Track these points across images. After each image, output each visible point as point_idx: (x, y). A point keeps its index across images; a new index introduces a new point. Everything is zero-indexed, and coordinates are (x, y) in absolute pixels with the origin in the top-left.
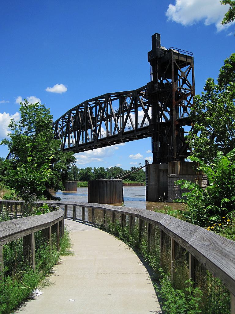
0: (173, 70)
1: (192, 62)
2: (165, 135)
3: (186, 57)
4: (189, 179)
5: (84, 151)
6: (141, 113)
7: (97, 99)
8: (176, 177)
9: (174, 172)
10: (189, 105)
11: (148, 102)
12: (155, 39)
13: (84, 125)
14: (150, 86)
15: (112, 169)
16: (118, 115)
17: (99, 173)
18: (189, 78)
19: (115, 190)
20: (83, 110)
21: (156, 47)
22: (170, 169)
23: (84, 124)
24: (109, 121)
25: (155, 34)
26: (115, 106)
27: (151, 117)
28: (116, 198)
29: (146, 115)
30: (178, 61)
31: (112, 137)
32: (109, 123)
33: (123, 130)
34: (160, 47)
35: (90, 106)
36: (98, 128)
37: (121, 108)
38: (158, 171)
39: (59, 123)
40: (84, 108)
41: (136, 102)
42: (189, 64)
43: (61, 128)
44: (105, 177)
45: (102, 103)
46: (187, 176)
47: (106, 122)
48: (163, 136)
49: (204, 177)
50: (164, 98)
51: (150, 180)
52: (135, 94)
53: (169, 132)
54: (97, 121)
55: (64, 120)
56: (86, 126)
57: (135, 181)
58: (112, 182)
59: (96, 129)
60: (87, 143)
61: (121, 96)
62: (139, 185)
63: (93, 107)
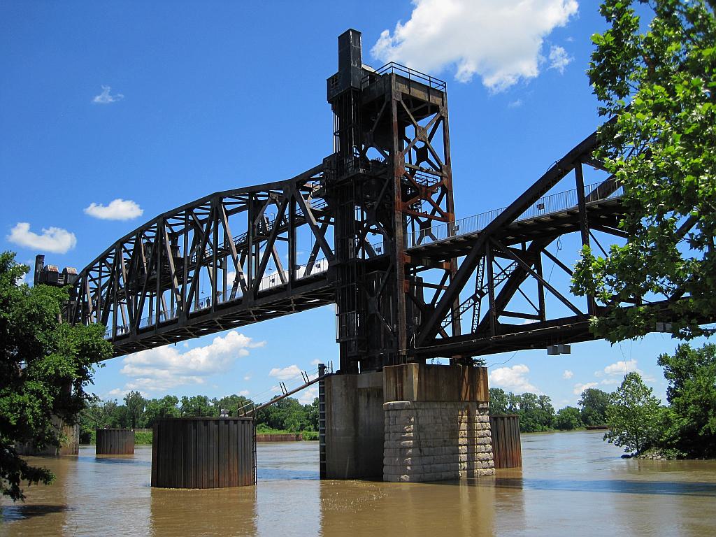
0: (395, 120)
1: (443, 105)
2: (372, 294)
3: (429, 90)
4: (443, 414)
5: (152, 347)
6: (305, 236)
7: (189, 209)
8: (408, 409)
9: (402, 396)
10: (437, 214)
11: (325, 212)
12: (348, 45)
13: (153, 277)
14: (333, 166)
15: (226, 401)
16: (244, 248)
18: (437, 144)
19: (232, 447)
20: (152, 240)
21: (350, 62)
22: (389, 387)
24: (220, 267)
25: (348, 32)
26: (237, 226)
27: (332, 247)
28: (236, 471)
29: (321, 243)
30: (409, 100)
31: (226, 306)
32: (220, 271)
33: (258, 287)
34: (359, 64)
35: (171, 230)
36: (189, 286)
37: (253, 229)
38: (354, 395)
39: (91, 276)
40: (154, 234)
41: (293, 209)
42: (435, 109)
43: (96, 290)
45: (202, 222)
46: (436, 406)
47: (211, 268)
48: (369, 297)
49: (483, 408)
50: (368, 196)
51: (333, 419)
52: (291, 191)
53: (385, 285)
54: (188, 265)
55: (105, 269)
56: (158, 279)
57: (280, 429)
58: (223, 423)
59: (184, 289)
60: (160, 325)
61: (252, 200)
62: (292, 440)
63: (180, 233)
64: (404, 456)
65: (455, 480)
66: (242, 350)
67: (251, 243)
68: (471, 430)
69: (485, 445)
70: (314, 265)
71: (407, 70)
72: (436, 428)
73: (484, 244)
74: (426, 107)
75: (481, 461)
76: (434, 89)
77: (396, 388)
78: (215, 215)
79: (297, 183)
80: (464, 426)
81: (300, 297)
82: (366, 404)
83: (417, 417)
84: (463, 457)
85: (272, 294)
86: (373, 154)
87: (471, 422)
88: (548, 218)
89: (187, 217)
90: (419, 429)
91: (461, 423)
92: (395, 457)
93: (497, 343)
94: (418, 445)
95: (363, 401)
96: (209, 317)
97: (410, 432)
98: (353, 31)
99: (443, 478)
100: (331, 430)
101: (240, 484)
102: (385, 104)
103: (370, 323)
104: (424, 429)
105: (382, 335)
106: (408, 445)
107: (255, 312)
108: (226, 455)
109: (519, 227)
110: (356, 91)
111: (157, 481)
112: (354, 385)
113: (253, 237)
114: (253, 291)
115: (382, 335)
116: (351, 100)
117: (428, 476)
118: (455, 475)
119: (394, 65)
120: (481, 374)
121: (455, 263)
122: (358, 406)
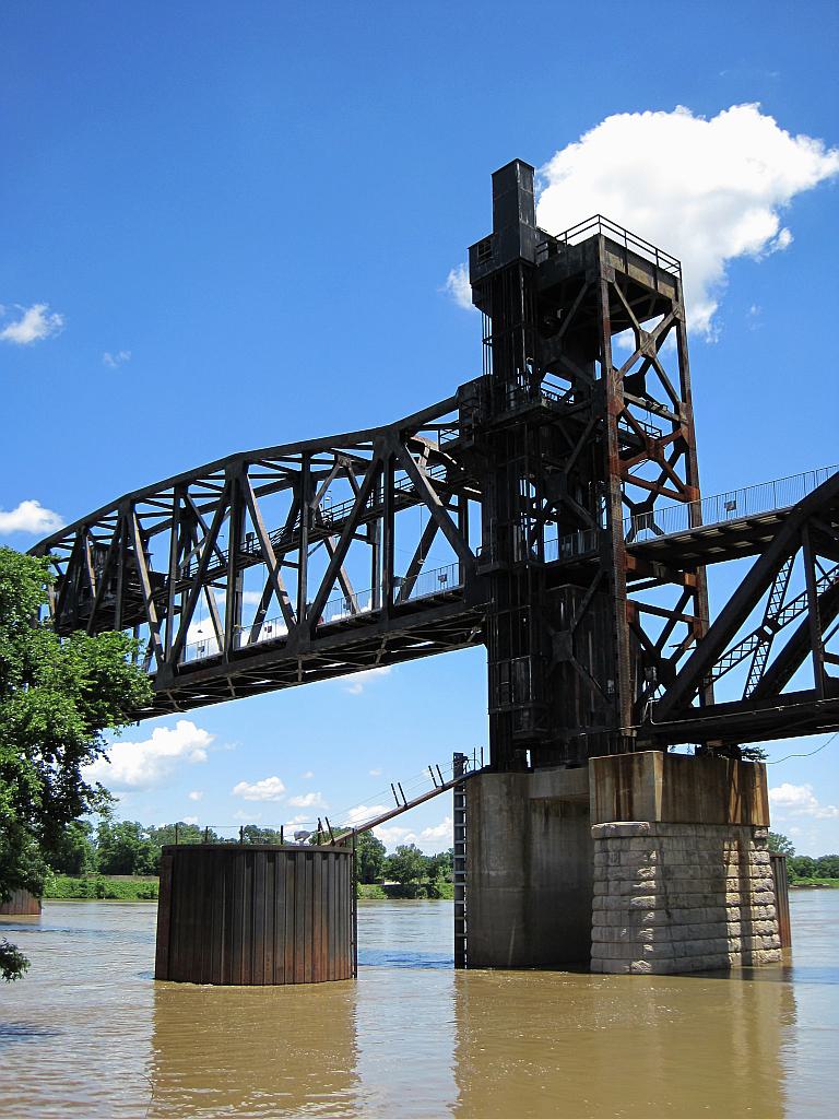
1: (677, 300)
3: (655, 270)
7: (181, 484)
8: (645, 836)
9: (631, 812)
10: (669, 484)
13: (107, 604)
14: (478, 399)
17: (120, 845)
22: (602, 795)
23: (108, 599)
25: (513, 163)
26: (272, 513)
28: (325, 951)
33: (317, 616)
38: (523, 809)
40: (112, 532)
42: (663, 305)
44: (141, 862)
48: (552, 632)
51: (483, 857)
52: (397, 441)
64: (637, 925)
65: (723, 970)
66: (197, 751)
67: (173, 588)
68: (744, 877)
69: (765, 905)
70: (263, 629)
71: (622, 233)
72: (691, 872)
73: (799, 531)
74: (649, 301)
75: (761, 935)
76: (663, 271)
77: (618, 796)
78: (233, 493)
79: (402, 433)
80: (733, 870)
81: (402, 635)
82: (543, 830)
83: (661, 853)
84: (735, 928)
85: (266, 651)
86: (555, 386)
87: (743, 862)
88: (716, 532)
89: (177, 503)
90: (666, 874)
91: (728, 864)
92: (621, 926)
93: (828, 711)
94: (665, 905)
95: (537, 822)
96: (218, 672)
97: (649, 879)
98: (522, 164)
99: (704, 967)
100: (480, 874)
101: (332, 977)
102: (586, 287)
103: (553, 676)
104: (673, 874)
105: (577, 702)
106: (646, 905)
107: (176, 696)
108: (309, 918)
109: (666, 546)
110: (528, 267)
111: (167, 969)
112: (524, 792)
113: (309, 528)
114: (306, 622)
115: (577, 702)
116: (519, 280)
117: (682, 963)
118: (723, 960)
119: (602, 221)
120: (757, 775)
121: (702, 577)
122: (531, 832)
